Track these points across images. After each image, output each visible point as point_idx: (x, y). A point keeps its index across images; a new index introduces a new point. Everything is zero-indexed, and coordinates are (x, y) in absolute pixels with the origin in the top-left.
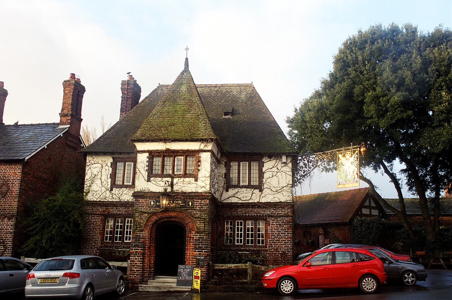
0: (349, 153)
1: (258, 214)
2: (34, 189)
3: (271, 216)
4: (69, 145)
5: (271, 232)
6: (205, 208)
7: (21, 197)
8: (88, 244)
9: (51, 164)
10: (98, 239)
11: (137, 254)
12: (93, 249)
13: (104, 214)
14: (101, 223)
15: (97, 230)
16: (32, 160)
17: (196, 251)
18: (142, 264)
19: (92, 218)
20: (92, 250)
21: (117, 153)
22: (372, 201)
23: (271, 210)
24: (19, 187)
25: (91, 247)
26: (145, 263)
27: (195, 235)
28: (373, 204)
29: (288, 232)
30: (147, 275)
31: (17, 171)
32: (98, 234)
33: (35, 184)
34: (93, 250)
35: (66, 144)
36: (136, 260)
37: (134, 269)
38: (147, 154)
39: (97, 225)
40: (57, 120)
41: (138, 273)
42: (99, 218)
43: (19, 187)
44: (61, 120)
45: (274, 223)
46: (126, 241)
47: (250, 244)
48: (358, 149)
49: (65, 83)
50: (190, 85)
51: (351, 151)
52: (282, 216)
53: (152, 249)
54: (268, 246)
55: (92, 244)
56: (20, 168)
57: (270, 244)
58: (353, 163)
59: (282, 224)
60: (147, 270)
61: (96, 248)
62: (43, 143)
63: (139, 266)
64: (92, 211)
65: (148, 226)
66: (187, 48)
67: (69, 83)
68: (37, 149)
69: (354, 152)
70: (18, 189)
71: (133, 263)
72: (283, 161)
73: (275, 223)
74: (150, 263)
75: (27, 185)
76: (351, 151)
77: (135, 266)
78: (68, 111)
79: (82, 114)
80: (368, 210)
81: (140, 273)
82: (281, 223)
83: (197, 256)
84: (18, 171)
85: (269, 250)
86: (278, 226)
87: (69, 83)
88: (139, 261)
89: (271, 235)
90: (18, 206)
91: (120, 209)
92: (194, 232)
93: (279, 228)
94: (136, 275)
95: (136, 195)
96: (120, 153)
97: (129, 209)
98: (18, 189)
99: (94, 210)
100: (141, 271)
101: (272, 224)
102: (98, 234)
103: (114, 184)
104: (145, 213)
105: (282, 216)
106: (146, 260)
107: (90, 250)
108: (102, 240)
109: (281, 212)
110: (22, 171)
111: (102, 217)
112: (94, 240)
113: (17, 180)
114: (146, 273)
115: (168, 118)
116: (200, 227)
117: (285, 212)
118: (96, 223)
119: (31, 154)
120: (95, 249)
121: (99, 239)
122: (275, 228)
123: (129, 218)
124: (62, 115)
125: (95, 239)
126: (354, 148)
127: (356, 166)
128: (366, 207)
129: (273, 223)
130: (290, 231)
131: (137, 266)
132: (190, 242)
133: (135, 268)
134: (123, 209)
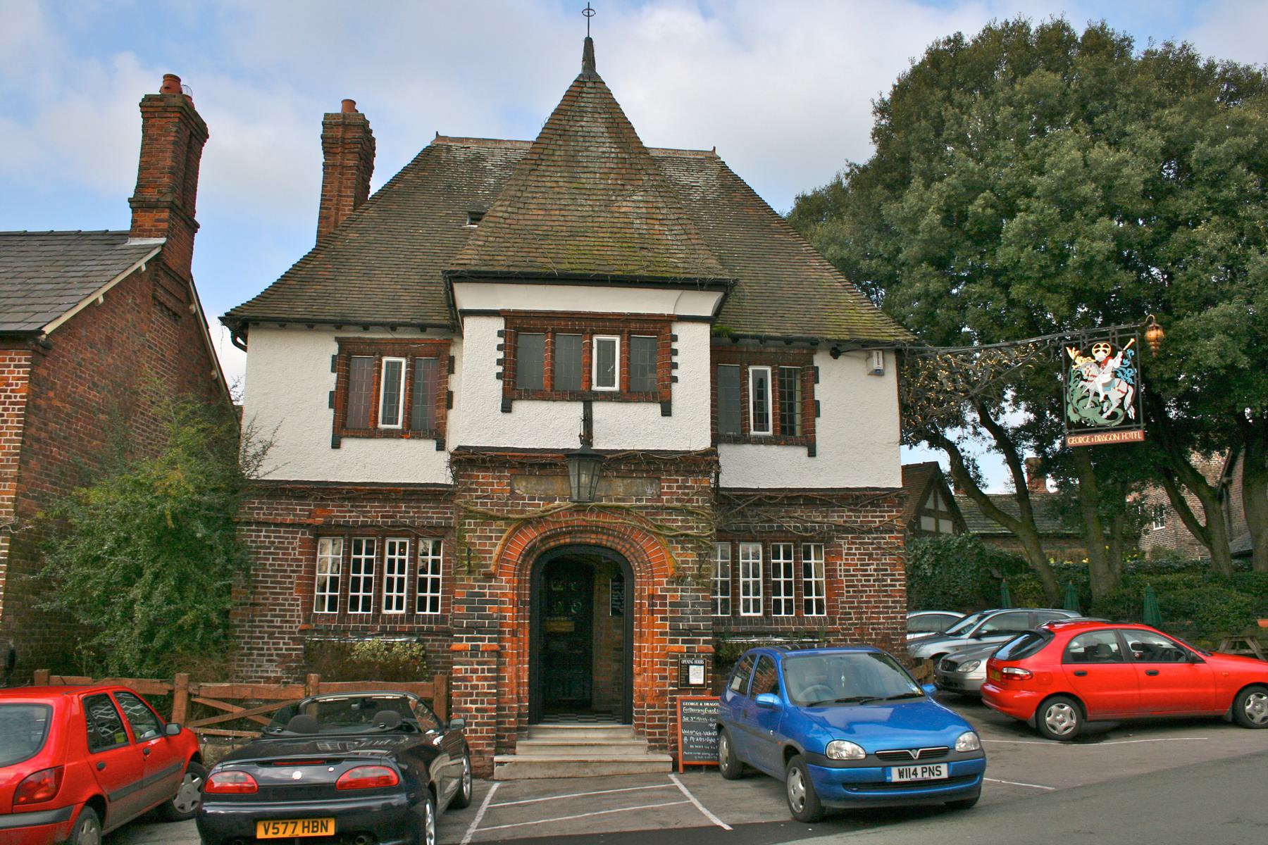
0: (1105, 346)
1: (807, 522)
2: (65, 438)
3: (847, 531)
4: (161, 304)
5: (845, 576)
6: (698, 502)
7: (27, 463)
8: (260, 621)
9: (113, 357)
10: (293, 605)
11: (476, 656)
12: (277, 638)
13: (309, 525)
14: (301, 553)
15: (290, 577)
16: (60, 338)
17: (676, 641)
18: (496, 687)
19: (270, 537)
20: (274, 644)
21: (356, 324)
22: (939, 496)
23: (843, 511)
24: (19, 428)
25: (271, 635)
26: (504, 685)
27: (668, 590)
28: (942, 507)
29: (894, 575)
30: (510, 723)
31: (9, 372)
32: (291, 588)
33: (68, 422)
34: (278, 643)
35: (154, 298)
36: (474, 676)
37: (469, 705)
38: (499, 324)
39: (287, 560)
40: (122, 220)
41: (482, 717)
42: (295, 538)
43: (19, 428)
44: (134, 221)
45: (854, 551)
46: (389, 612)
47: (783, 614)
48: (1137, 333)
49: (149, 104)
50: (614, 119)
51: (1114, 339)
52: (877, 530)
53: (525, 636)
54: (840, 619)
55: (273, 621)
56: (23, 362)
57: (842, 613)
58: (1120, 374)
59: (877, 554)
60: (511, 708)
61: (287, 636)
62: (111, 273)
63: (486, 694)
64: (271, 514)
65: (508, 562)
66: (589, 9)
67: (162, 104)
68: (77, 304)
69: (1123, 342)
70: (16, 434)
71: (466, 687)
72: (875, 366)
73: (856, 549)
74: (519, 685)
75: (46, 425)
76: (1114, 339)
77: (471, 694)
78: (160, 192)
79: (197, 208)
80: (933, 520)
81: (492, 717)
82: (874, 549)
83: (682, 656)
84: (13, 372)
85: (843, 629)
86: (864, 560)
87: (162, 104)
88: (485, 679)
89: (847, 586)
90: (17, 494)
91: (366, 507)
92: (665, 580)
93: (868, 565)
94: (477, 724)
95: (466, 460)
96: (366, 327)
97: (397, 507)
98: (16, 434)
99: (277, 509)
100: (491, 710)
101: (847, 554)
102: (291, 588)
103: (344, 425)
104: (497, 518)
105: (877, 530)
106: (508, 674)
107: (268, 643)
108: (308, 607)
109: (875, 518)
110: (30, 373)
111: (304, 533)
112: (280, 610)
113: (11, 403)
114: (507, 716)
115: (560, 210)
116: (683, 562)
117: (882, 517)
118: (283, 554)
119: (60, 316)
120: (284, 638)
121: (298, 605)
122: (856, 565)
123: (397, 536)
124: (138, 204)
125: (284, 605)
126: (1121, 331)
127: (1130, 380)
128: (929, 513)
129: (849, 555)
130: (899, 575)
131: (477, 695)
132: (653, 612)
133: (472, 702)
134: (377, 507)
